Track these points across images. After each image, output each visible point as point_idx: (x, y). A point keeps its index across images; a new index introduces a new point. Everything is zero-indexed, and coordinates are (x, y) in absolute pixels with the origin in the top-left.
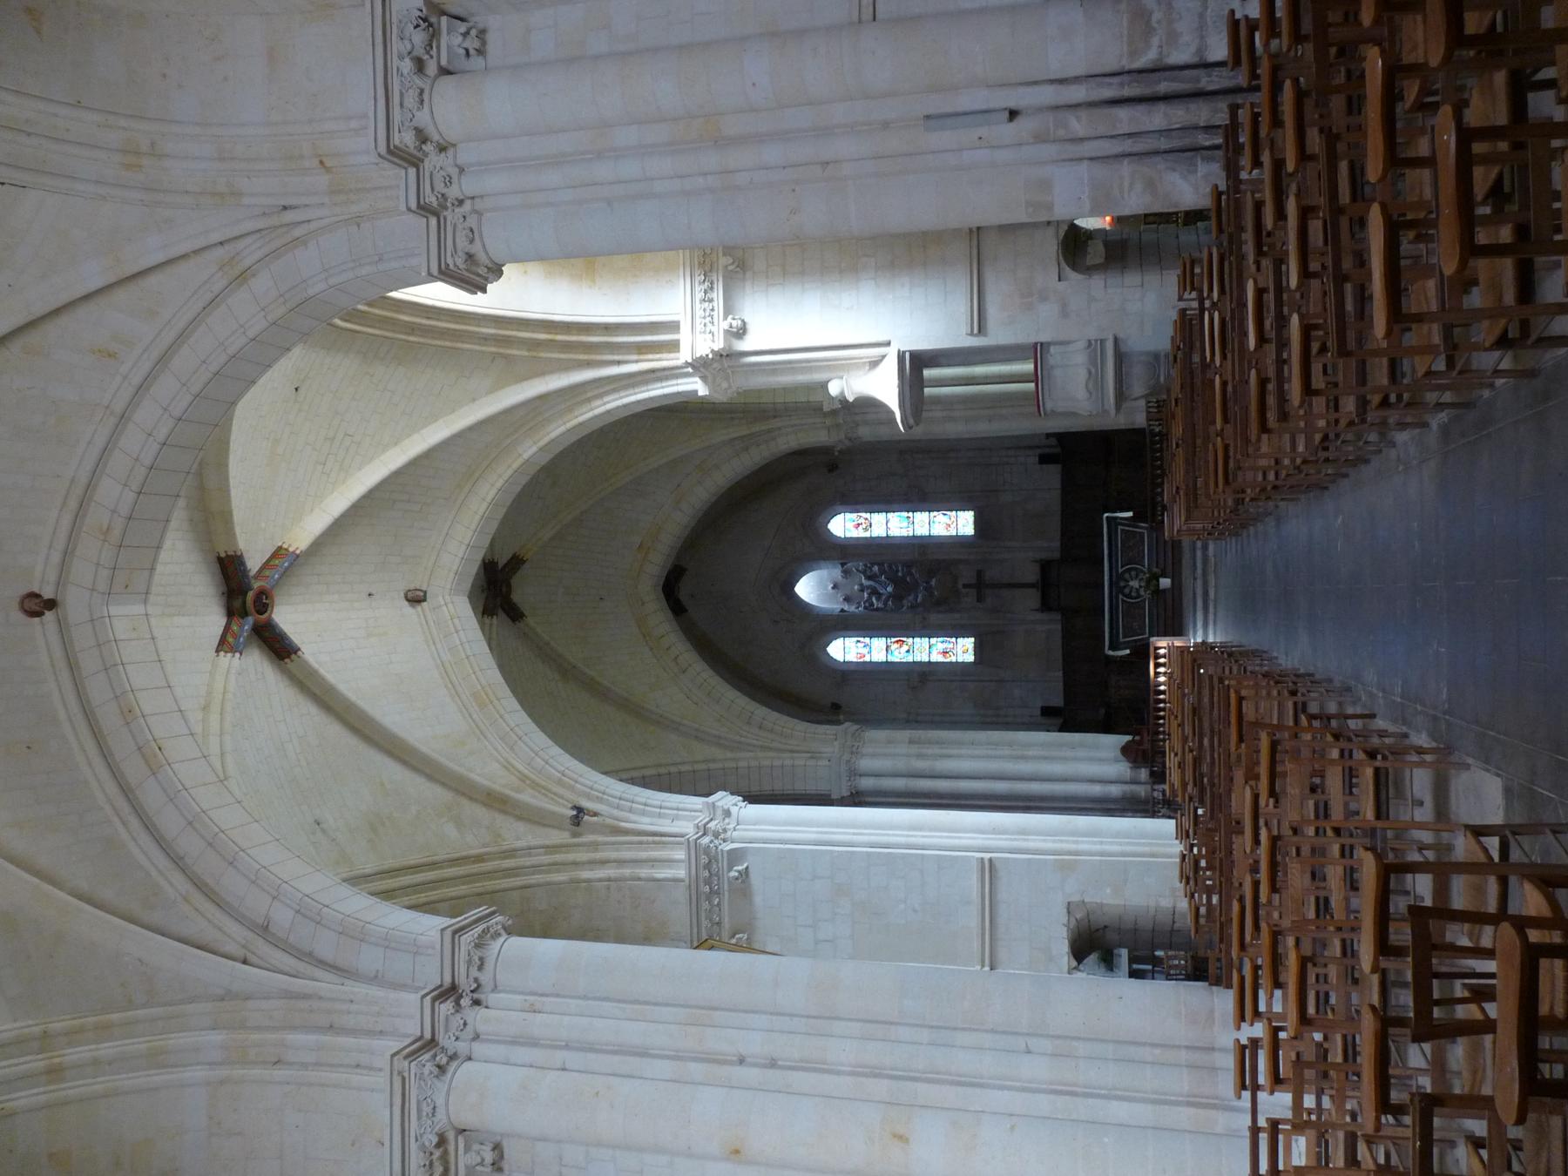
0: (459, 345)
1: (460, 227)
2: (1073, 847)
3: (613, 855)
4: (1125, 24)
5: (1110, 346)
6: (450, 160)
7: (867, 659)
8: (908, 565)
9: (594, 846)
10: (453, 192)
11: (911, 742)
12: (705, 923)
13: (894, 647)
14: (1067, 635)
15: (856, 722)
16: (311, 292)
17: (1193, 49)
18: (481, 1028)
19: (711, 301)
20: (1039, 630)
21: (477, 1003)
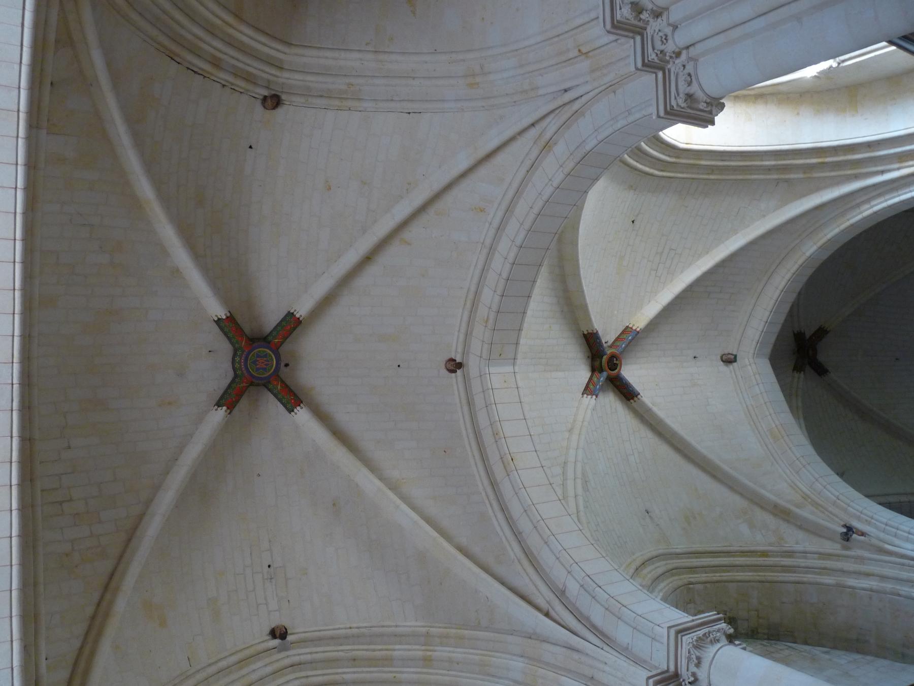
1: (681, 74)
3: (876, 569)
9: (861, 560)
10: (670, 47)
16: (588, 148)
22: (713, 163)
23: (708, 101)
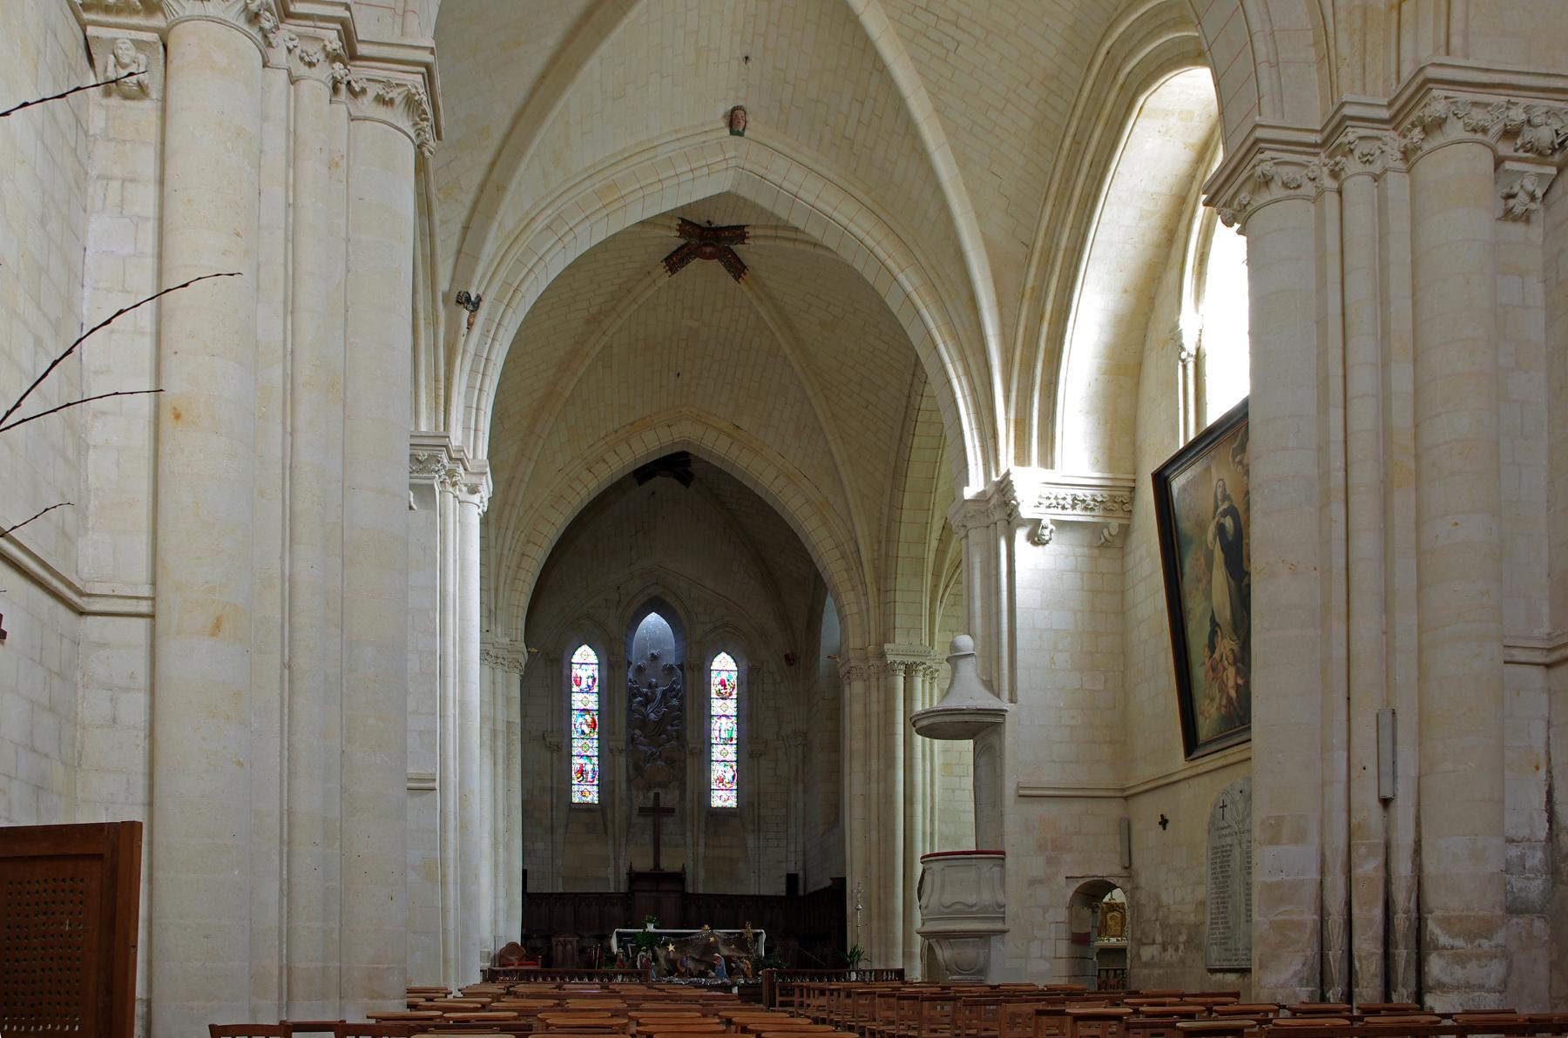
2: (451, 878)
5: (998, 926)
6: (1391, 164)
7: (575, 689)
8: (680, 737)
10: (1352, 165)
13: (587, 717)
14: (603, 898)
17: (1446, 979)
18: (304, 85)
19: (1074, 507)
20: (607, 868)
21: (335, 89)
23: (1249, 208)
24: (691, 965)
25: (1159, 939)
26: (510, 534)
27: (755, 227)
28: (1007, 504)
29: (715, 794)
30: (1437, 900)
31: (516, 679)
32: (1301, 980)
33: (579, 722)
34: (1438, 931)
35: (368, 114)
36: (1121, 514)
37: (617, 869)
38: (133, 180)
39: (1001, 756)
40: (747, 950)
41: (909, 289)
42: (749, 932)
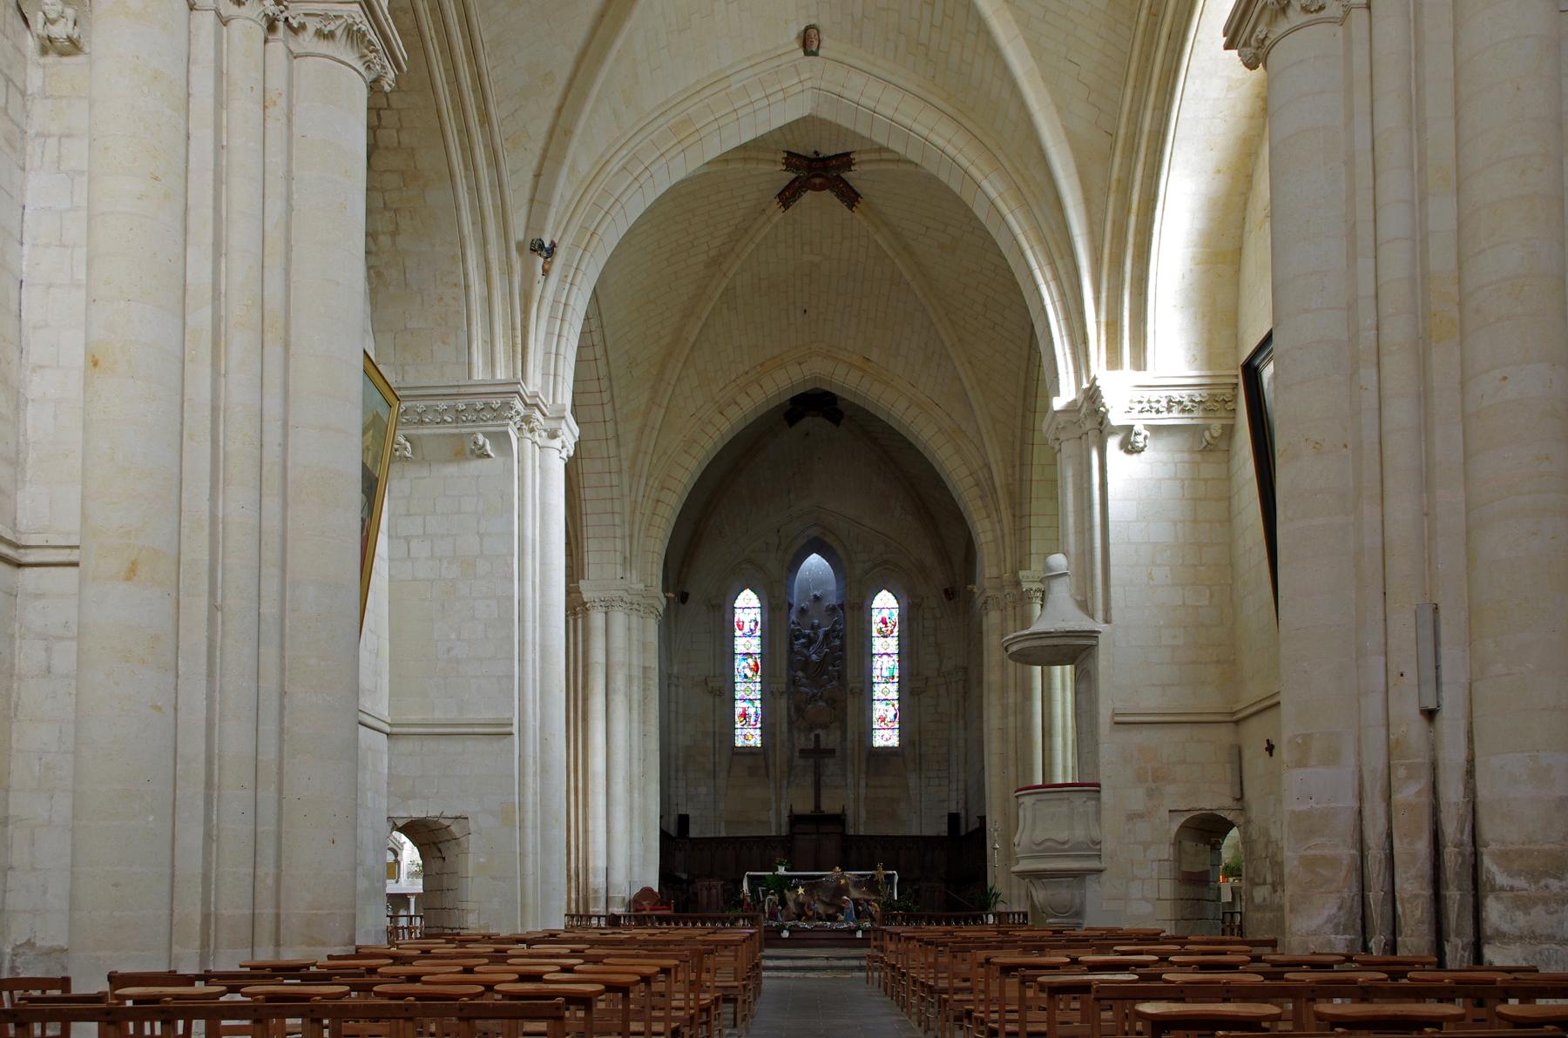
0: (1131, 82)
2: (529, 824)
4: (1547, 847)
7: (738, 633)
8: (841, 676)
11: (645, 668)
12: (421, 405)
13: (751, 661)
15: (667, 609)
17: (1505, 927)
19: (1169, 409)
20: (768, 812)
21: (271, 27)
22: (1168, 18)
23: (1267, 43)
24: (820, 908)
25: (1269, 879)
26: (643, 481)
27: (860, 152)
28: (1097, 411)
29: (877, 734)
30: (1495, 833)
31: (653, 627)
32: (1337, 926)
33: (742, 666)
34: (1494, 868)
35: (311, 49)
36: (1223, 414)
37: (778, 812)
38: (69, 136)
39: (1096, 680)
40: (877, 892)
41: (993, 194)
42: (880, 873)
